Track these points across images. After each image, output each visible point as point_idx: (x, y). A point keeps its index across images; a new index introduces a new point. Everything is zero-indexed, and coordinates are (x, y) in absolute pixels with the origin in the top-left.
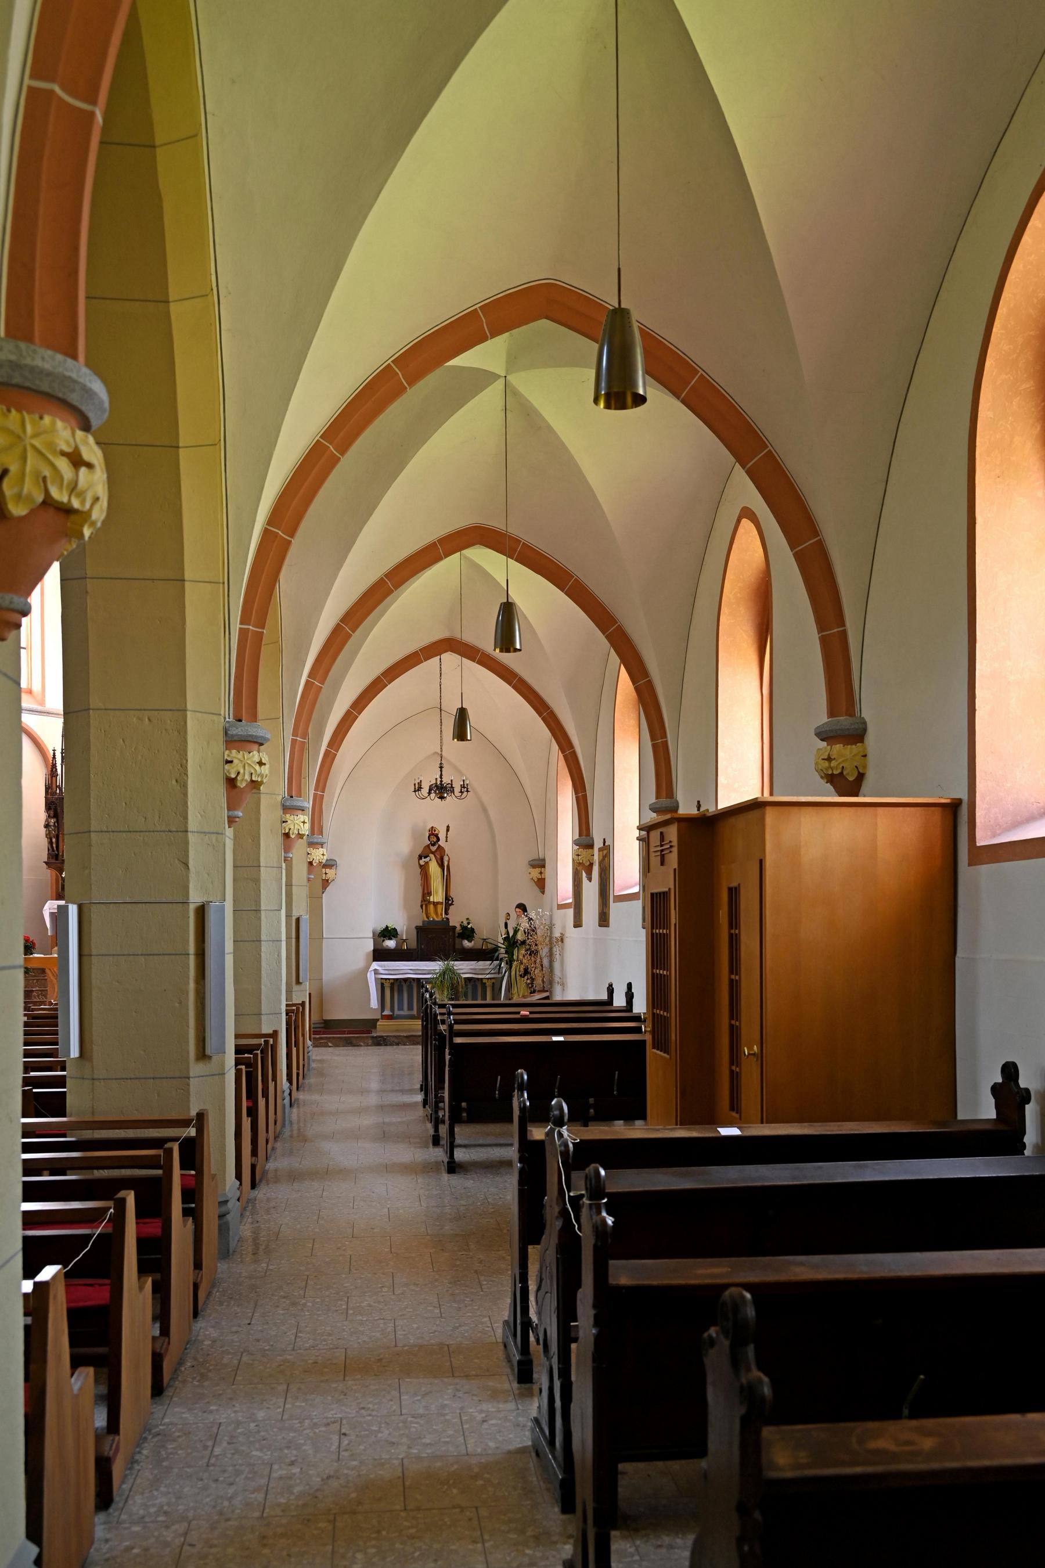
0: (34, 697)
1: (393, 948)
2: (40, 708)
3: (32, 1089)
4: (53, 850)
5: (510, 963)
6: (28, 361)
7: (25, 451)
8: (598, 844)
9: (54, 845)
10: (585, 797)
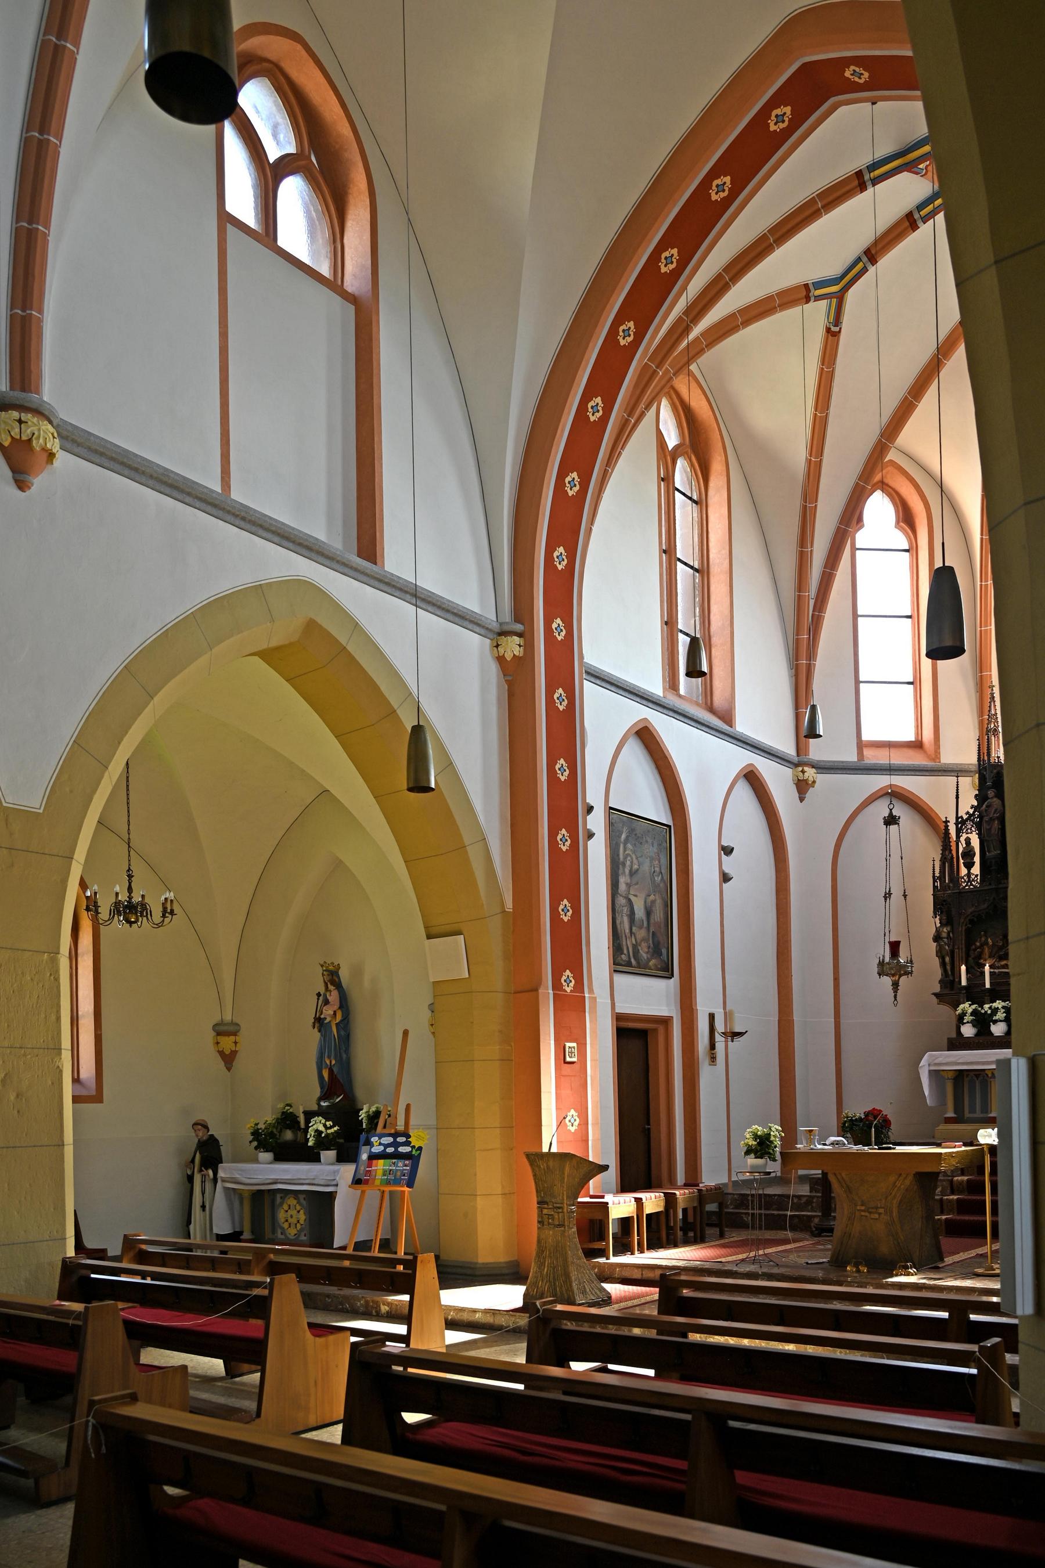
0: (925, 752)
1: (402, 1132)
9: (948, 968)
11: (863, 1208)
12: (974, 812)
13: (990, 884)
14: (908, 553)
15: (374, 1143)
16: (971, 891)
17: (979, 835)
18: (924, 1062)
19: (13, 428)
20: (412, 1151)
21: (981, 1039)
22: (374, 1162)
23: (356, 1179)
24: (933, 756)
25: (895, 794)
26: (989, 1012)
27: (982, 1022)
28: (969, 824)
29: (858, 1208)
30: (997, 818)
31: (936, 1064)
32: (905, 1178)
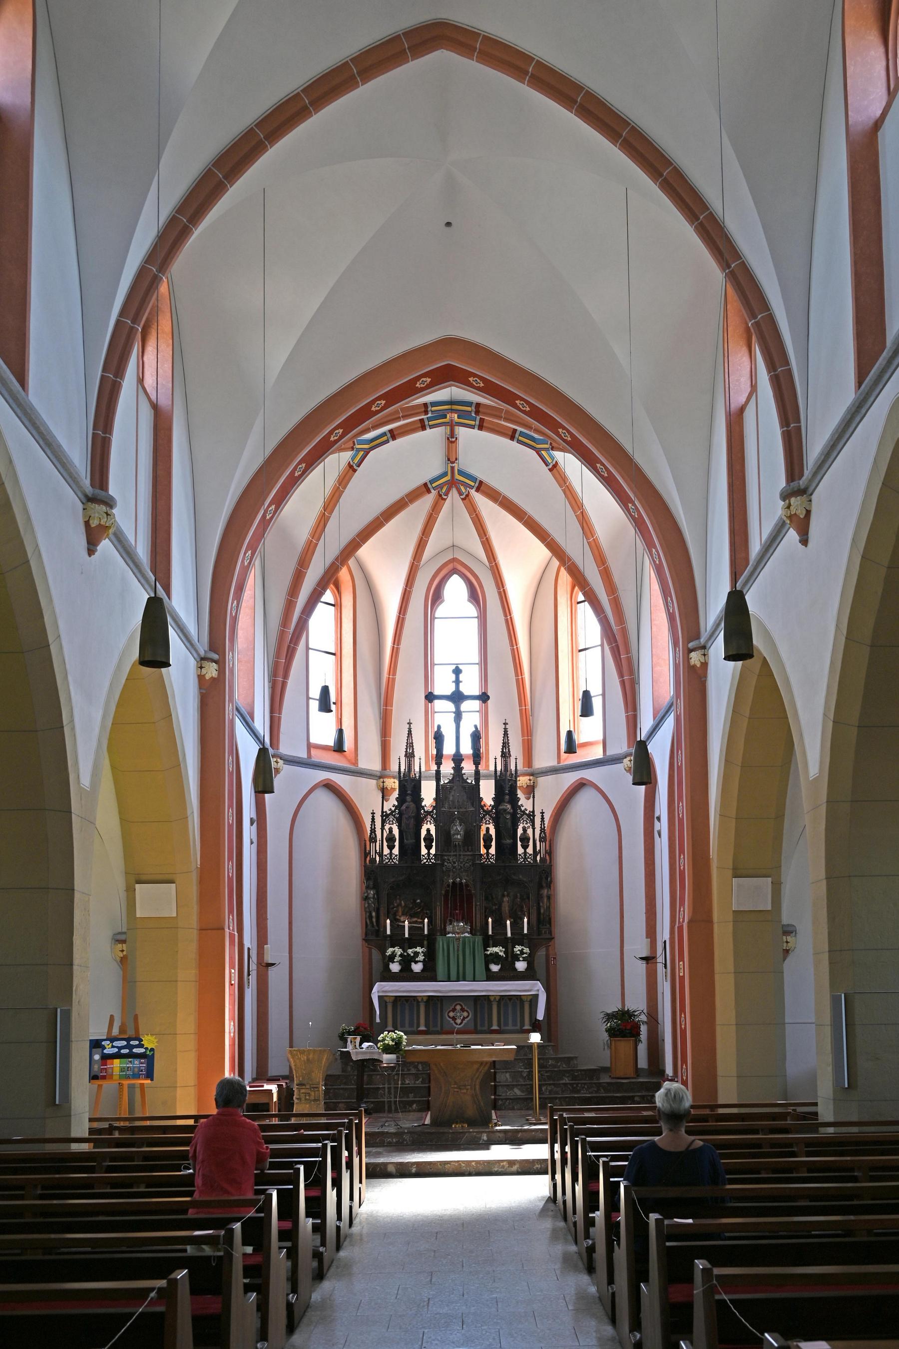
0: (345, 757)
2: (352, 767)
3: (573, 1126)
4: (373, 926)
11: (456, 1086)
12: (395, 810)
13: (406, 863)
14: (333, 607)
15: (106, 1046)
16: (391, 866)
17: (399, 827)
18: (375, 989)
19: (103, 518)
20: (146, 1052)
21: (405, 974)
22: (109, 1061)
23: (91, 1076)
24: (354, 762)
25: (329, 786)
26: (412, 955)
27: (406, 962)
28: (391, 818)
29: (452, 1086)
30: (413, 817)
31: (383, 991)
32: (485, 1066)
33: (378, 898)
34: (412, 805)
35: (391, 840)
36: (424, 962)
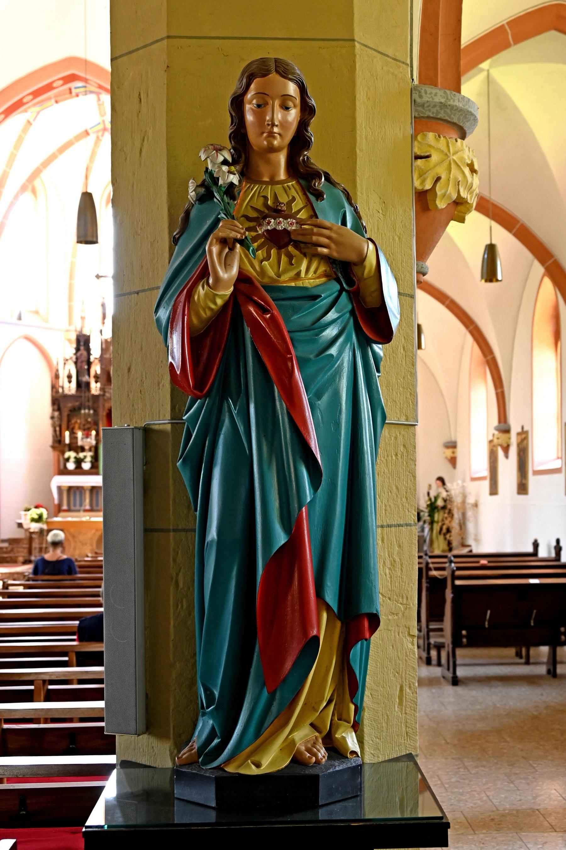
5: (432, 523)
6: (451, 103)
7: (450, 164)
8: (515, 429)
10: (503, 393)
21: (78, 470)
27: (79, 462)
33: (61, 418)
34: (85, 353)
35: (69, 377)
36: (91, 462)
